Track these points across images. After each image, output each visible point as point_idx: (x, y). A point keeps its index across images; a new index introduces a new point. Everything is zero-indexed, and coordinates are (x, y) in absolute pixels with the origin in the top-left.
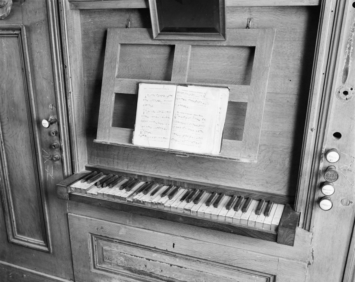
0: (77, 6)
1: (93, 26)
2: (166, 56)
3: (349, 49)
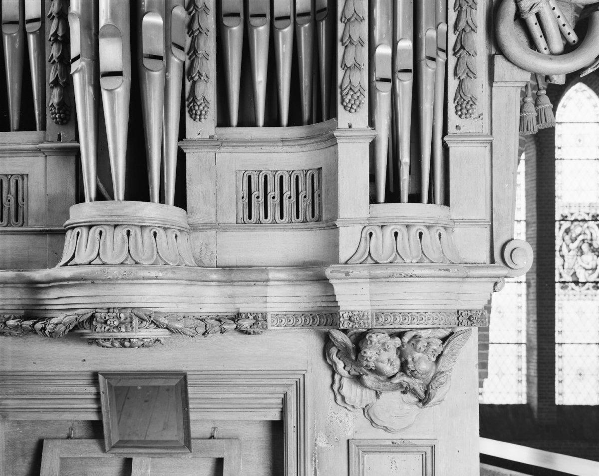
0: (5, 417)
1: (22, 435)
2: (119, 468)
3: (315, 461)
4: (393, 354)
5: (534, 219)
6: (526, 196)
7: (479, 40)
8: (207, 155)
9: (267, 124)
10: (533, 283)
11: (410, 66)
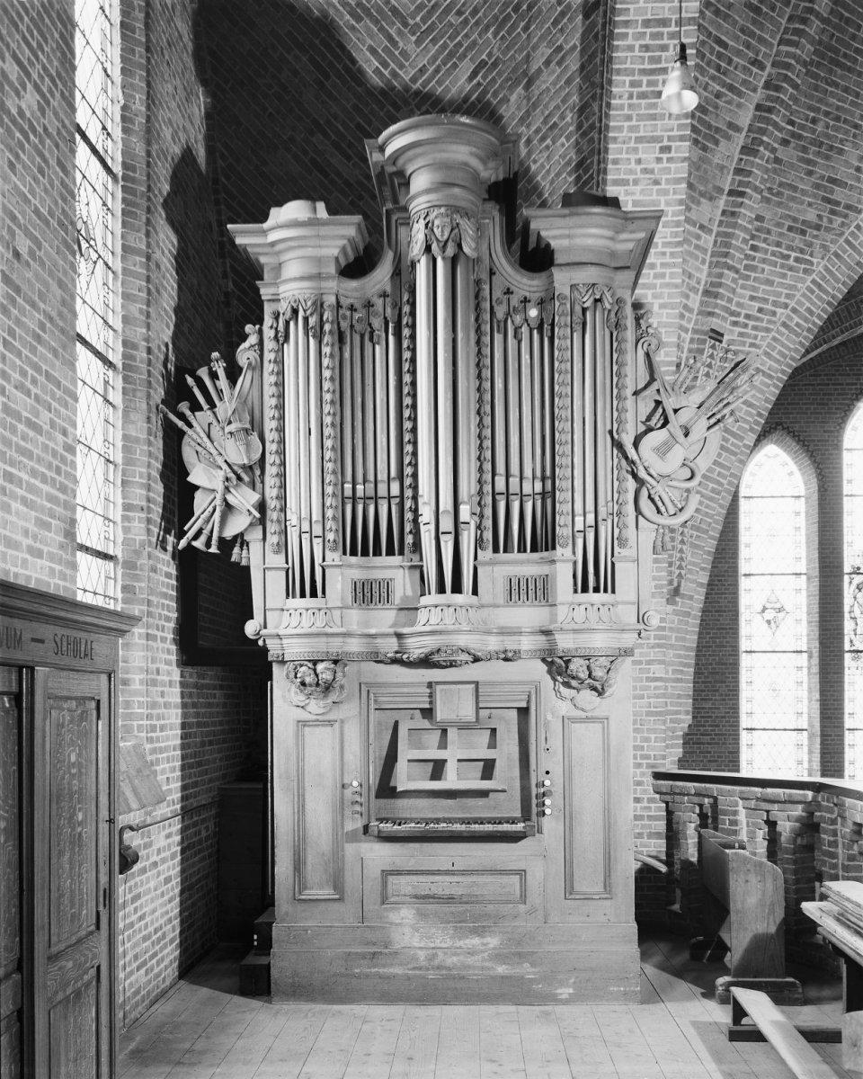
4: (585, 668)
5: (817, 573)
6: (807, 543)
7: (630, 507)
8: (489, 568)
9: (519, 551)
10: (816, 654)
11: (593, 524)
